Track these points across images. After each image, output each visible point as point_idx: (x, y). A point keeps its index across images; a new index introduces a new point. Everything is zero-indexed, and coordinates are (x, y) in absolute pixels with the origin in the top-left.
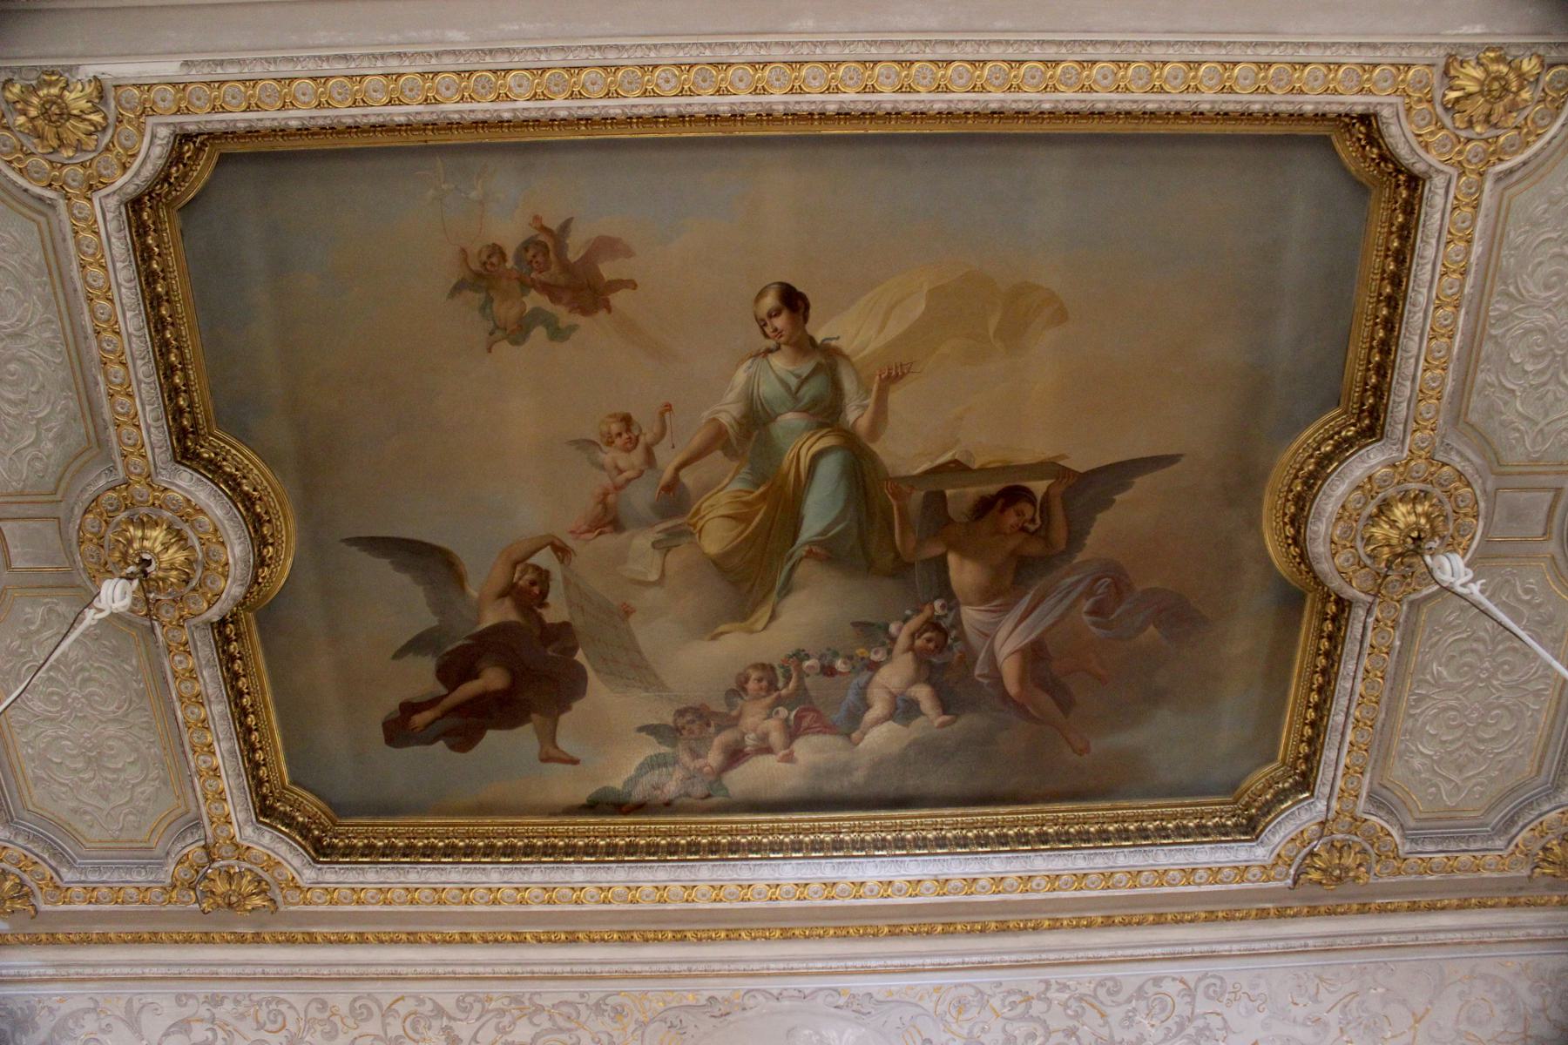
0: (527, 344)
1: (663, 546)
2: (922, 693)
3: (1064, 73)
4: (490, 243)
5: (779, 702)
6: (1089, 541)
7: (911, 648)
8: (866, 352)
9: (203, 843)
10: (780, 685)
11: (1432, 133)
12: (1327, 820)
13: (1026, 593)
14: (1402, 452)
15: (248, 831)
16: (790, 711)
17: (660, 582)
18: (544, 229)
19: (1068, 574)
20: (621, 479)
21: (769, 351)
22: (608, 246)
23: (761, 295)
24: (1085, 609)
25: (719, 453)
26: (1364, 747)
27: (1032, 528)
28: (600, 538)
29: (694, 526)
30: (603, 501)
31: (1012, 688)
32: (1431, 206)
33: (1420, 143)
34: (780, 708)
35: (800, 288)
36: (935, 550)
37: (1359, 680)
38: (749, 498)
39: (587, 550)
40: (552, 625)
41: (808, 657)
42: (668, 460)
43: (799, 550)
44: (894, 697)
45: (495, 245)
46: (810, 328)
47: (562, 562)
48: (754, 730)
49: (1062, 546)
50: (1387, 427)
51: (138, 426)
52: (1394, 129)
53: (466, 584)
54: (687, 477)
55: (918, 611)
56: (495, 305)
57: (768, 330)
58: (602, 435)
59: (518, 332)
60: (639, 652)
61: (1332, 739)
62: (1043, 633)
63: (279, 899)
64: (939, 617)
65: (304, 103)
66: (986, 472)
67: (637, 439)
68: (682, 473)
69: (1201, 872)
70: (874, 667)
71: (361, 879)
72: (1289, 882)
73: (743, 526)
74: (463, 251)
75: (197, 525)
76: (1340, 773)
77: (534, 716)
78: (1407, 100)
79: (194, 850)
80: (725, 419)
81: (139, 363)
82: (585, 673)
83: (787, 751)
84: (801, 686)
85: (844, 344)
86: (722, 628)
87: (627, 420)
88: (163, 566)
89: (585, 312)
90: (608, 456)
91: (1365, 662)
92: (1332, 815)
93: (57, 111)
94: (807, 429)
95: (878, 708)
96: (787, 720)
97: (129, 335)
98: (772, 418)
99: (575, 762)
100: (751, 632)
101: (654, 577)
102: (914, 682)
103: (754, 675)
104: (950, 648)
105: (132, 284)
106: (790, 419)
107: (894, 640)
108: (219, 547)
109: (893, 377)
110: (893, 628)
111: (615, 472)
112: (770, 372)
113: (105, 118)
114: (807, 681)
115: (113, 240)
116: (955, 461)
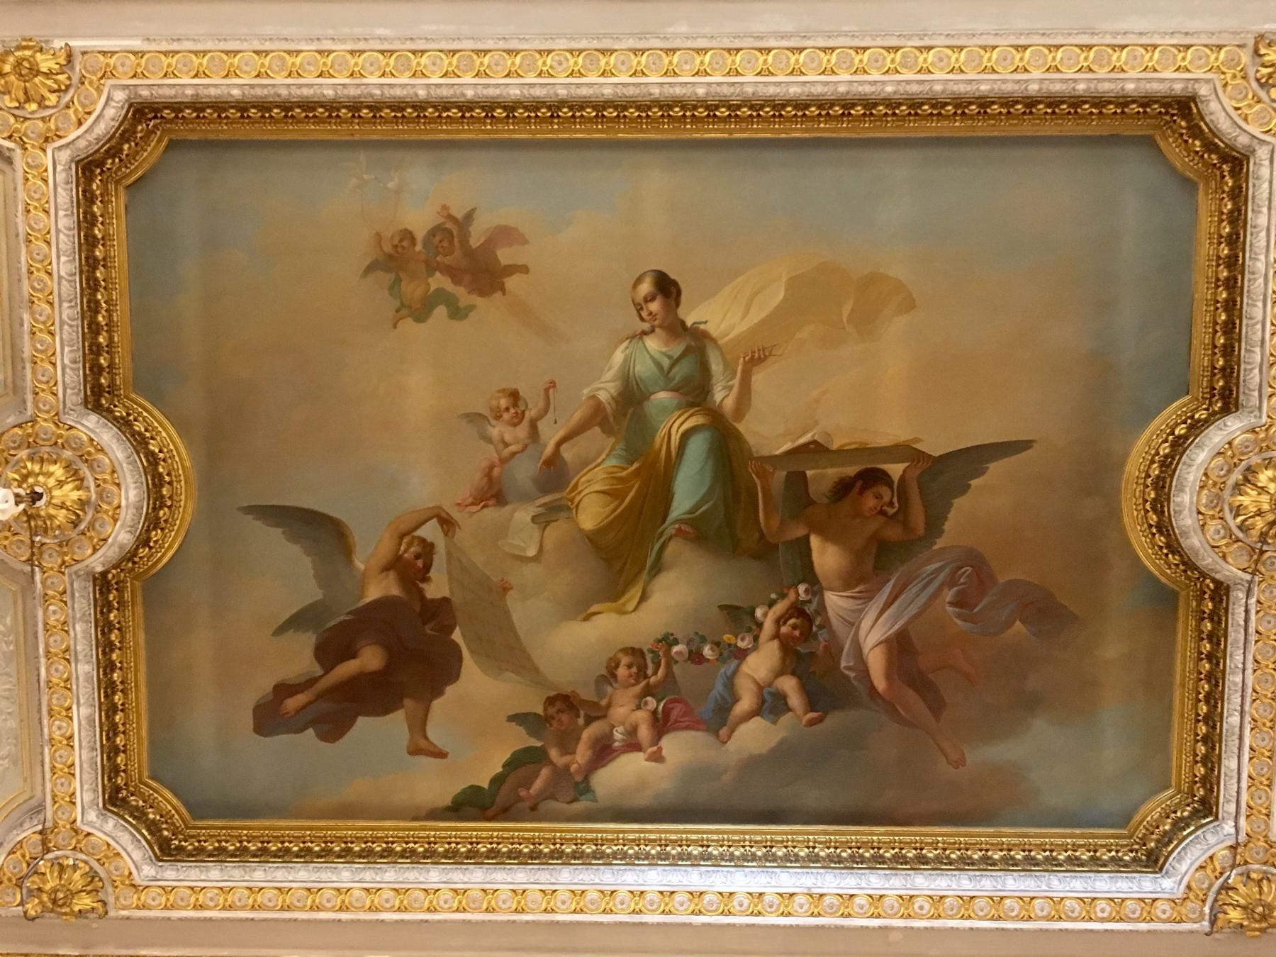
0: (430, 321)
1: (542, 521)
2: (788, 685)
3: (904, 56)
4: (401, 227)
5: (648, 691)
6: (947, 526)
7: (776, 635)
8: (731, 336)
9: (40, 827)
10: (649, 672)
11: (1250, 106)
12: (1238, 844)
13: (888, 580)
14: (1260, 417)
15: (92, 816)
16: (658, 702)
17: (536, 559)
18: (451, 217)
19: (929, 561)
20: (506, 452)
21: (644, 333)
22: (506, 234)
23: (639, 281)
24: (948, 599)
25: (597, 429)
26: (1268, 754)
27: (891, 511)
28: (485, 510)
29: (572, 500)
30: (488, 474)
31: (880, 683)
32: (1258, 179)
33: (1240, 115)
34: (649, 699)
35: (673, 276)
36: (800, 532)
37: (1249, 671)
38: (624, 473)
39: (472, 523)
40: (433, 601)
41: (676, 642)
42: (551, 434)
43: (669, 528)
44: (760, 688)
45: (406, 230)
46: (681, 312)
47: (446, 534)
48: (623, 724)
49: (921, 531)
50: (1241, 397)
51: (54, 364)
52: (1214, 106)
53: (353, 556)
54: (568, 453)
55: (783, 596)
56: (403, 283)
57: (644, 314)
58: (492, 410)
59: (421, 312)
60: (515, 633)
61: (1230, 744)
62: (907, 623)
63: (111, 900)
64: (804, 602)
65: (246, 72)
66: (843, 455)
67: (523, 412)
68: (564, 447)
69: (1102, 904)
70: (742, 654)
71: (203, 877)
72: (1206, 924)
73: (616, 503)
74: (378, 234)
75: (95, 466)
76: (1244, 784)
77: (408, 702)
78: (1222, 77)
79: (29, 832)
80: (603, 396)
81: (65, 305)
82: (460, 652)
83: (655, 748)
84: (669, 674)
85: (712, 329)
86: (594, 608)
87: (514, 396)
88: (54, 501)
89: (483, 293)
90: (495, 431)
91: (1252, 648)
92: (1242, 838)
93: (28, 66)
94: (679, 407)
95: (746, 703)
96: (655, 712)
97: (60, 277)
98: (647, 397)
99: (442, 755)
100: (622, 612)
101: (531, 552)
102: (780, 673)
103: (625, 660)
104: (815, 637)
105: (71, 233)
106: (663, 396)
107: (760, 625)
108: (115, 489)
109: (756, 360)
110: (759, 613)
111: (501, 446)
112: (646, 353)
113: (69, 78)
114: (676, 669)
115: (59, 190)
116: (814, 442)
